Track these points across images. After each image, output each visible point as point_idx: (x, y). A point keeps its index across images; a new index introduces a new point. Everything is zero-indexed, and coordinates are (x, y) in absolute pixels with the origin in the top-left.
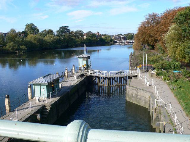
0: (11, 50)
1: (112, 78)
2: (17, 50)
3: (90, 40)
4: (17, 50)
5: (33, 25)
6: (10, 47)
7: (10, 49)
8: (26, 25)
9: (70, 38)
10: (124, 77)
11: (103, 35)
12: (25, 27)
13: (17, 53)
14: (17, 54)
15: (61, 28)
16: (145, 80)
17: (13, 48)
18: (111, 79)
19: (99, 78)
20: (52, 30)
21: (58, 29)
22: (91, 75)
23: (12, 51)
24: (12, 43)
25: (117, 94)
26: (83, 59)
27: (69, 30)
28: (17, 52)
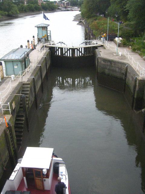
1: (77, 49)
18: (76, 50)
19: (62, 49)
26: (43, 29)
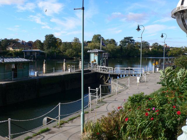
0: (70, 56)
2: (74, 56)
3: (155, 51)
4: (74, 56)
5: (100, 35)
6: (69, 53)
7: (69, 54)
8: (94, 36)
9: (131, 48)
10: (120, 75)
11: (171, 47)
12: (92, 37)
13: (74, 59)
14: (75, 60)
15: (125, 38)
16: (36, 48)
17: (71, 54)
20: (114, 39)
21: (122, 38)
22: (104, 73)
23: (70, 57)
24: (70, 50)
25: (17, 80)
27: (133, 40)
28: (75, 58)
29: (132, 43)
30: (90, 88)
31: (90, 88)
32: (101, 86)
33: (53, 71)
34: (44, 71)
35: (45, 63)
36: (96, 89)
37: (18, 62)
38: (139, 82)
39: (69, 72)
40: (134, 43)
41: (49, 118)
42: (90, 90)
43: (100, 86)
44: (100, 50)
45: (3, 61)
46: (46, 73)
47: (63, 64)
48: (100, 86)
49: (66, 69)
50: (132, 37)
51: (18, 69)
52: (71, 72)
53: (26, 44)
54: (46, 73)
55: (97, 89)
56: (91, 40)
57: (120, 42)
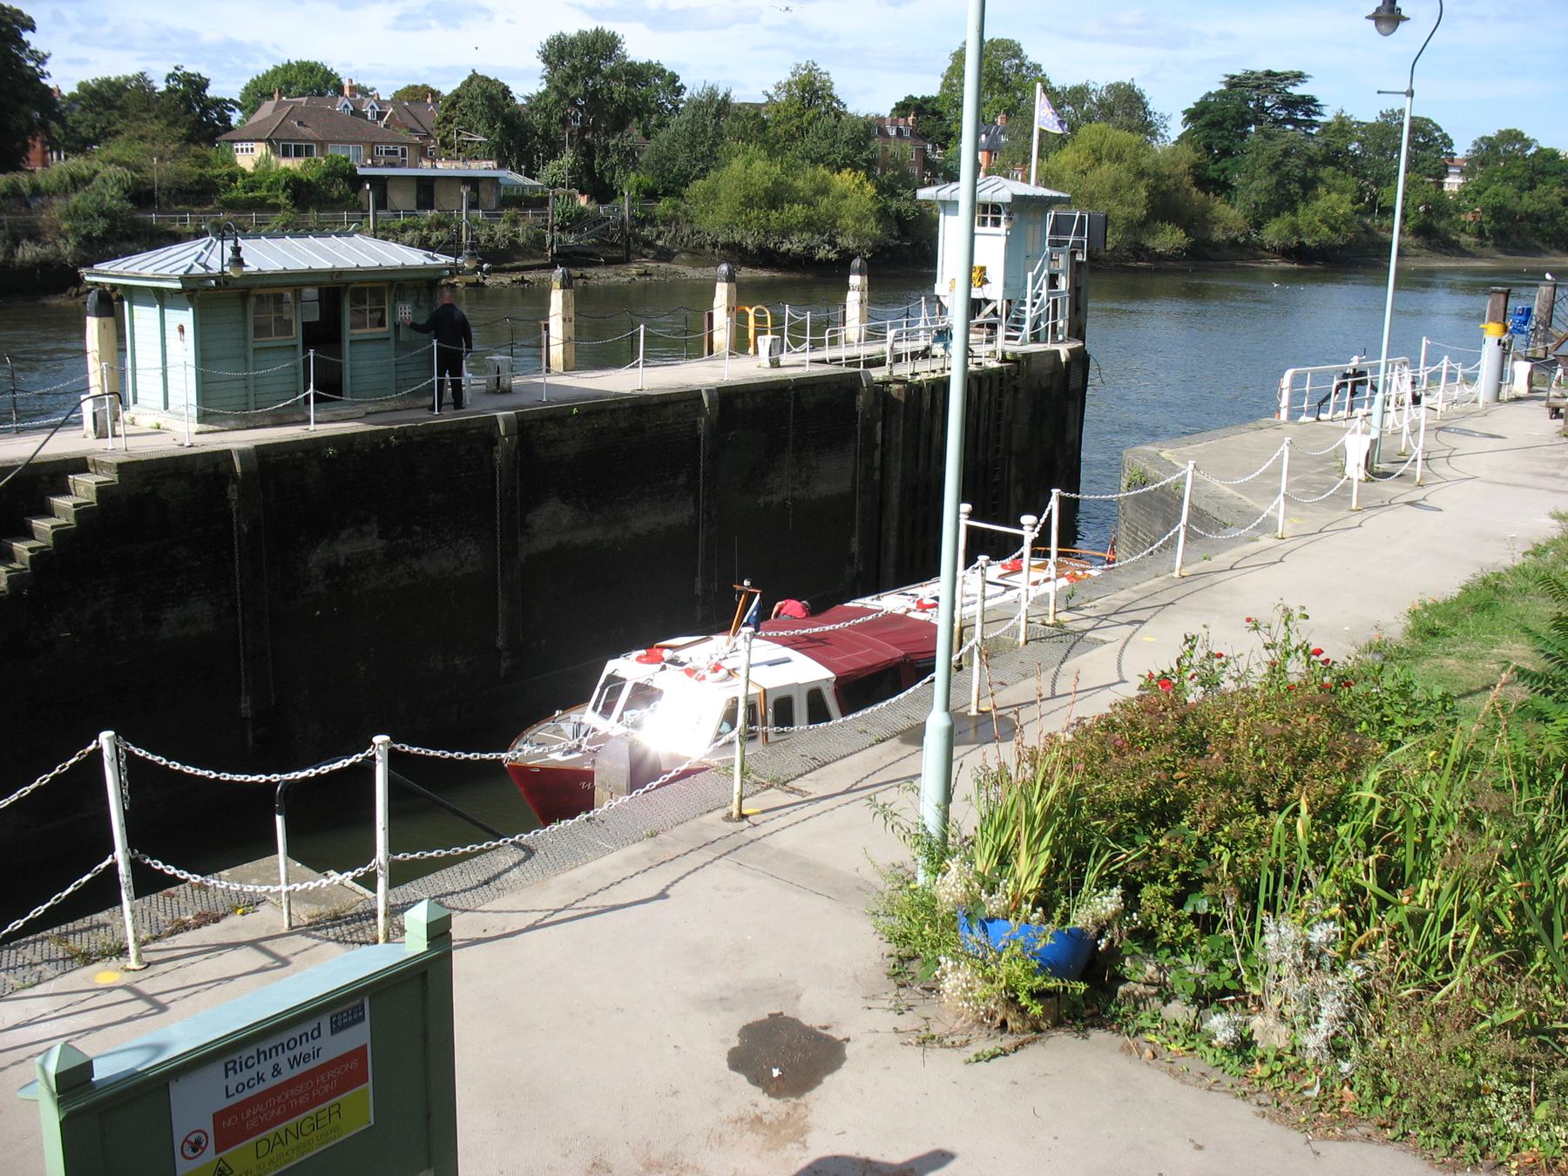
27: (1308, 103)
29: (1297, 123)
30: (972, 516)
31: (972, 516)
32: (1061, 499)
33: (633, 354)
34: (557, 352)
35: (563, 287)
36: (1020, 527)
37: (394, 270)
38: (1361, 474)
39: (752, 368)
40: (1313, 124)
41: (28, 789)
42: (969, 528)
43: (1054, 504)
44: (1026, 179)
45: (238, 261)
46: (567, 368)
47: (547, 304)
48: (1054, 504)
49: (740, 345)
50: (1299, 77)
51: (349, 333)
52: (775, 364)
53: (381, 116)
54: (567, 368)
55: (1028, 527)
56: (388, 98)
57: (1339, 117)
